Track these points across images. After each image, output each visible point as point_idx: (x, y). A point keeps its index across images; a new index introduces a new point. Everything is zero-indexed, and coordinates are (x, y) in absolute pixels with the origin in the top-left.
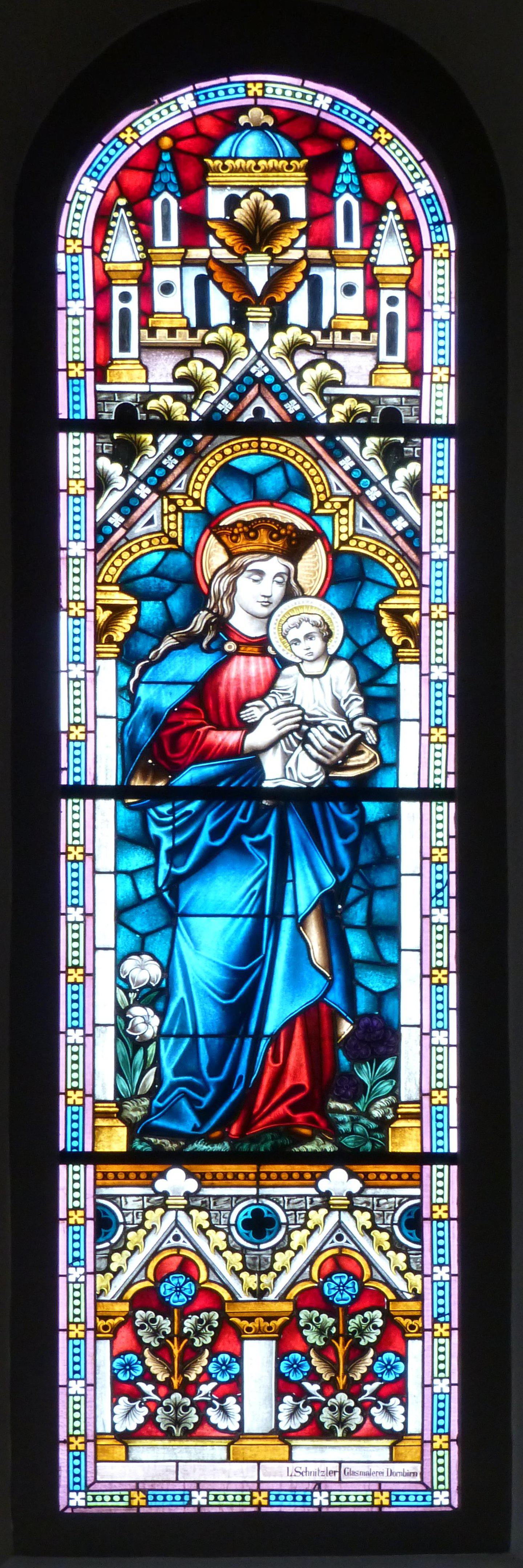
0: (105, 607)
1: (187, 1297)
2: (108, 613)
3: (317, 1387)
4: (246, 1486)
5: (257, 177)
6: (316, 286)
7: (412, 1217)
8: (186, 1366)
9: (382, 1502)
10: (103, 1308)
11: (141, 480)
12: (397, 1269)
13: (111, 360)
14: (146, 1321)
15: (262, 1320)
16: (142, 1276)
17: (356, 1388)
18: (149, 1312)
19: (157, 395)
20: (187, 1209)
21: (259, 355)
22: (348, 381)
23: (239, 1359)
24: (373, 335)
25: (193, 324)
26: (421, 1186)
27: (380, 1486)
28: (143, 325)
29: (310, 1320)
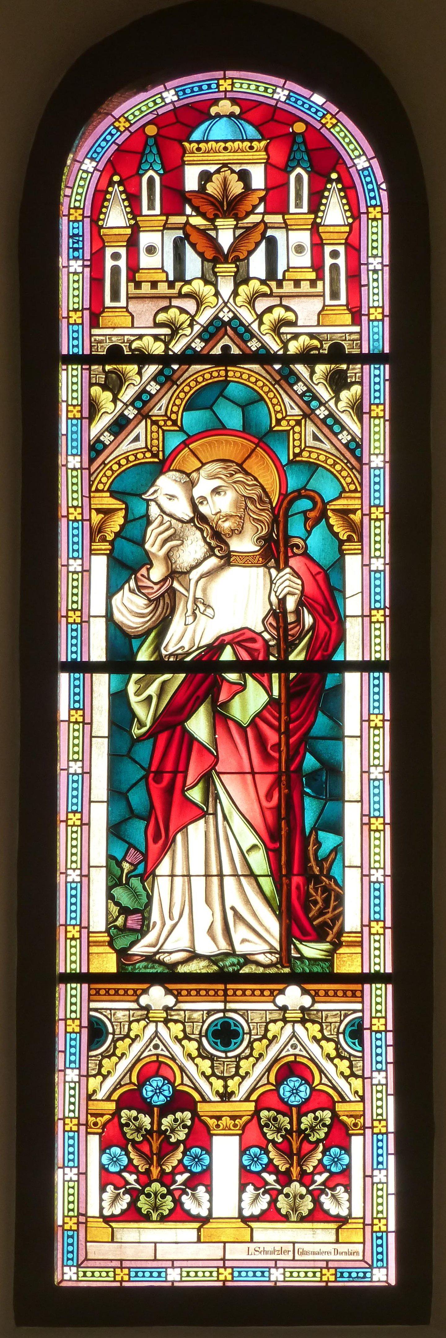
0: (99, 511)
1: (166, 1097)
2: (101, 516)
3: (134, 1177)
4: (109, 1264)
5: (225, 157)
6: (272, 244)
7: (355, 1028)
8: (303, 1158)
9: (226, 1277)
10: (93, 1106)
11: (126, 405)
12: (203, 1074)
13: (103, 308)
14: (269, 1119)
15: (228, 1118)
16: (264, 1080)
17: (308, 1177)
18: (132, 1111)
19: (140, 337)
20: (166, 1021)
21: (225, 304)
22: (299, 323)
23: (209, 1152)
24: (320, 284)
25: (171, 278)
26: (362, 1002)
27: (327, 1264)
28: (131, 278)
29: (129, 1119)
